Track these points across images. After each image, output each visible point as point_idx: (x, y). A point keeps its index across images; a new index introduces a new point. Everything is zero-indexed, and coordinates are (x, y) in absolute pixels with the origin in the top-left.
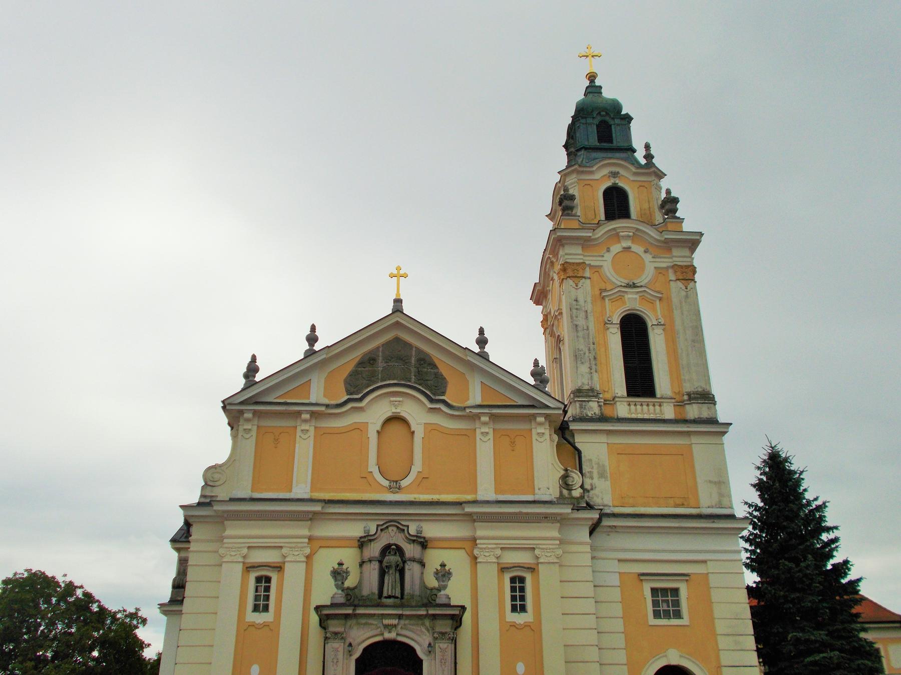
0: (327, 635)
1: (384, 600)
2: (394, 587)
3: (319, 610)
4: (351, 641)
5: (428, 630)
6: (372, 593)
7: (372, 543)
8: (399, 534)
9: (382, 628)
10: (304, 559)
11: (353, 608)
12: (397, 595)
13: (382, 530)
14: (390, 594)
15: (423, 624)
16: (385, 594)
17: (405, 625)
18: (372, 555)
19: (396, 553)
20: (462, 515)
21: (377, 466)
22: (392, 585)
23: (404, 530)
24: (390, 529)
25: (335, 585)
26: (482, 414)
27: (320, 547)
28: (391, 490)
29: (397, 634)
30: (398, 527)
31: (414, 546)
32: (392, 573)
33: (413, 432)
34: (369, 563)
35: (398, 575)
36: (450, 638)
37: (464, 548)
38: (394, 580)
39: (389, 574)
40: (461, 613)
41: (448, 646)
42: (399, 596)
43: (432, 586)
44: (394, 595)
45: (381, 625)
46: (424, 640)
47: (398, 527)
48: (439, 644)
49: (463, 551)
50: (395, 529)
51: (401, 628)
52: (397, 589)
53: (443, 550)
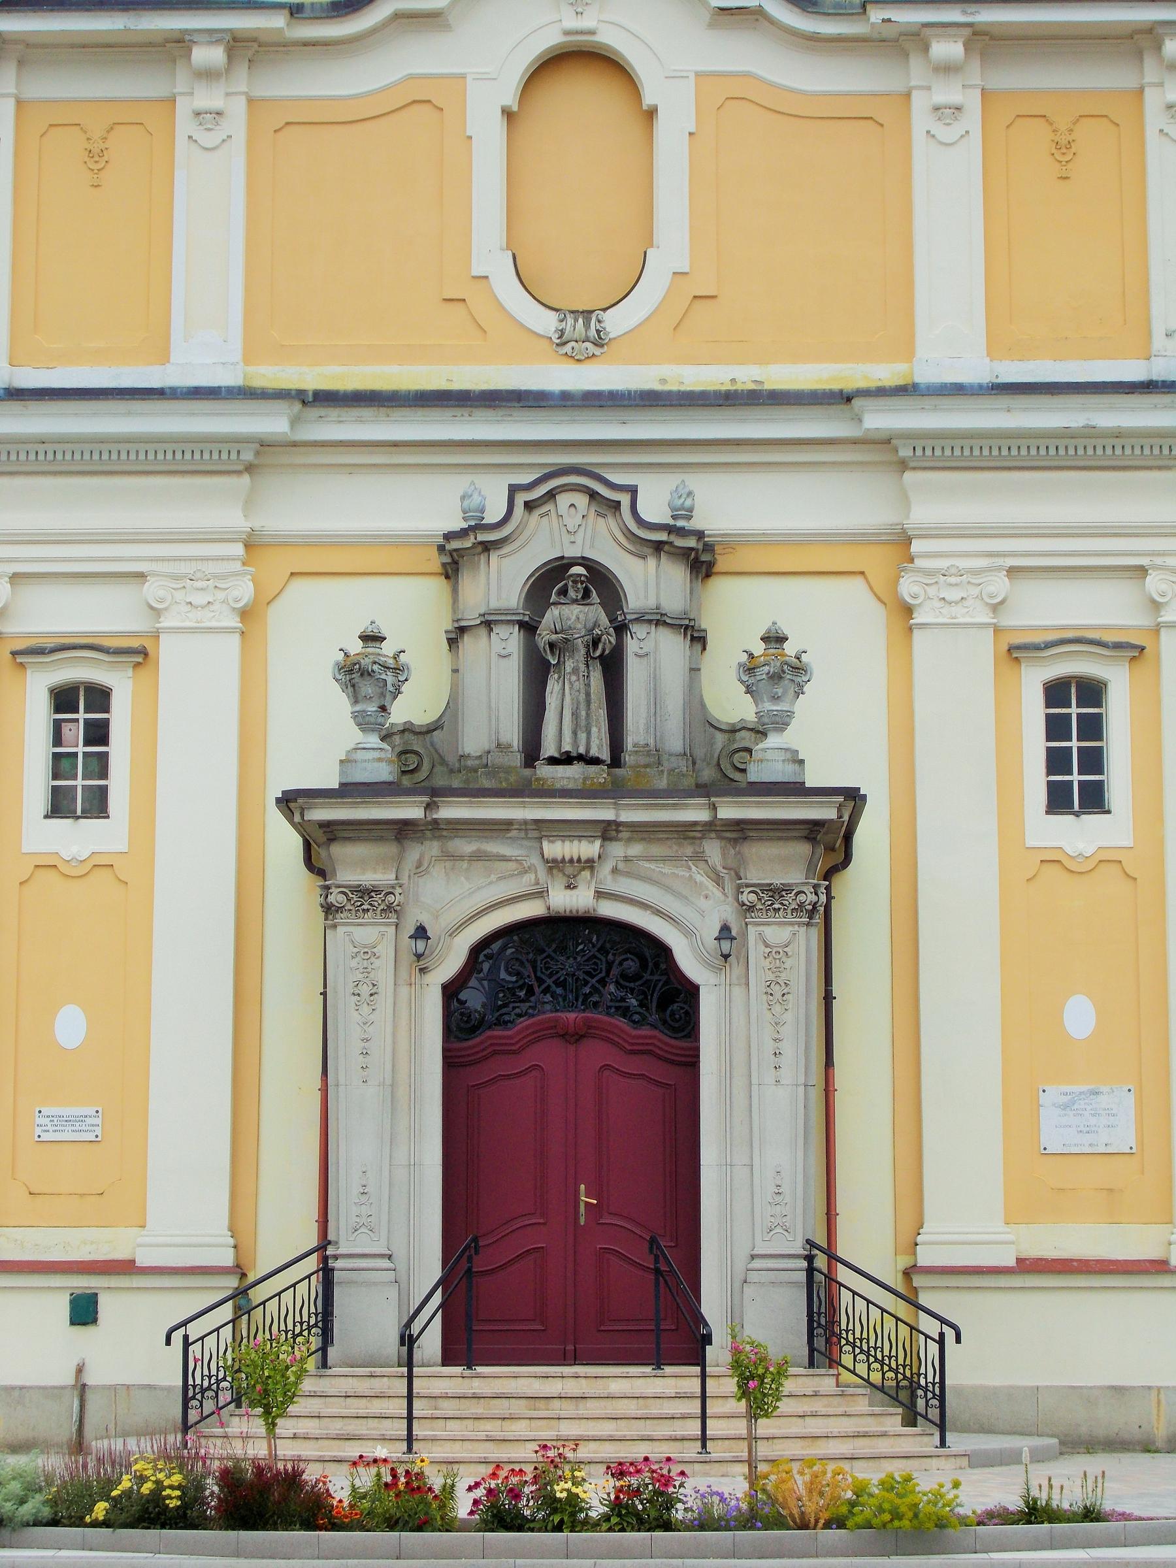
0: (331, 899)
1: (545, 771)
2: (583, 723)
4: (425, 919)
5: (718, 880)
6: (499, 745)
7: (494, 557)
8: (601, 520)
10: (234, 622)
11: (426, 799)
12: (594, 752)
13: (529, 506)
14: (567, 747)
15: (699, 857)
16: (549, 748)
17: (627, 859)
18: (494, 604)
19: (587, 594)
20: (855, 442)
21: (510, 253)
22: (575, 715)
23: (619, 502)
24: (564, 500)
26: (940, 31)
28: (567, 348)
29: (599, 895)
30: (593, 495)
31: (658, 566)
32: (575, 671)
33: (651, 114)
34: (483, 631)
37: (862, 573)
38: (582, 697)
39: (562, 678)
44: (582, 750)
45: (535, 860)
46: (702, 913)
47: (593, 495)
50: (582, 500)
51: (615, 871)
52: (594, 730)
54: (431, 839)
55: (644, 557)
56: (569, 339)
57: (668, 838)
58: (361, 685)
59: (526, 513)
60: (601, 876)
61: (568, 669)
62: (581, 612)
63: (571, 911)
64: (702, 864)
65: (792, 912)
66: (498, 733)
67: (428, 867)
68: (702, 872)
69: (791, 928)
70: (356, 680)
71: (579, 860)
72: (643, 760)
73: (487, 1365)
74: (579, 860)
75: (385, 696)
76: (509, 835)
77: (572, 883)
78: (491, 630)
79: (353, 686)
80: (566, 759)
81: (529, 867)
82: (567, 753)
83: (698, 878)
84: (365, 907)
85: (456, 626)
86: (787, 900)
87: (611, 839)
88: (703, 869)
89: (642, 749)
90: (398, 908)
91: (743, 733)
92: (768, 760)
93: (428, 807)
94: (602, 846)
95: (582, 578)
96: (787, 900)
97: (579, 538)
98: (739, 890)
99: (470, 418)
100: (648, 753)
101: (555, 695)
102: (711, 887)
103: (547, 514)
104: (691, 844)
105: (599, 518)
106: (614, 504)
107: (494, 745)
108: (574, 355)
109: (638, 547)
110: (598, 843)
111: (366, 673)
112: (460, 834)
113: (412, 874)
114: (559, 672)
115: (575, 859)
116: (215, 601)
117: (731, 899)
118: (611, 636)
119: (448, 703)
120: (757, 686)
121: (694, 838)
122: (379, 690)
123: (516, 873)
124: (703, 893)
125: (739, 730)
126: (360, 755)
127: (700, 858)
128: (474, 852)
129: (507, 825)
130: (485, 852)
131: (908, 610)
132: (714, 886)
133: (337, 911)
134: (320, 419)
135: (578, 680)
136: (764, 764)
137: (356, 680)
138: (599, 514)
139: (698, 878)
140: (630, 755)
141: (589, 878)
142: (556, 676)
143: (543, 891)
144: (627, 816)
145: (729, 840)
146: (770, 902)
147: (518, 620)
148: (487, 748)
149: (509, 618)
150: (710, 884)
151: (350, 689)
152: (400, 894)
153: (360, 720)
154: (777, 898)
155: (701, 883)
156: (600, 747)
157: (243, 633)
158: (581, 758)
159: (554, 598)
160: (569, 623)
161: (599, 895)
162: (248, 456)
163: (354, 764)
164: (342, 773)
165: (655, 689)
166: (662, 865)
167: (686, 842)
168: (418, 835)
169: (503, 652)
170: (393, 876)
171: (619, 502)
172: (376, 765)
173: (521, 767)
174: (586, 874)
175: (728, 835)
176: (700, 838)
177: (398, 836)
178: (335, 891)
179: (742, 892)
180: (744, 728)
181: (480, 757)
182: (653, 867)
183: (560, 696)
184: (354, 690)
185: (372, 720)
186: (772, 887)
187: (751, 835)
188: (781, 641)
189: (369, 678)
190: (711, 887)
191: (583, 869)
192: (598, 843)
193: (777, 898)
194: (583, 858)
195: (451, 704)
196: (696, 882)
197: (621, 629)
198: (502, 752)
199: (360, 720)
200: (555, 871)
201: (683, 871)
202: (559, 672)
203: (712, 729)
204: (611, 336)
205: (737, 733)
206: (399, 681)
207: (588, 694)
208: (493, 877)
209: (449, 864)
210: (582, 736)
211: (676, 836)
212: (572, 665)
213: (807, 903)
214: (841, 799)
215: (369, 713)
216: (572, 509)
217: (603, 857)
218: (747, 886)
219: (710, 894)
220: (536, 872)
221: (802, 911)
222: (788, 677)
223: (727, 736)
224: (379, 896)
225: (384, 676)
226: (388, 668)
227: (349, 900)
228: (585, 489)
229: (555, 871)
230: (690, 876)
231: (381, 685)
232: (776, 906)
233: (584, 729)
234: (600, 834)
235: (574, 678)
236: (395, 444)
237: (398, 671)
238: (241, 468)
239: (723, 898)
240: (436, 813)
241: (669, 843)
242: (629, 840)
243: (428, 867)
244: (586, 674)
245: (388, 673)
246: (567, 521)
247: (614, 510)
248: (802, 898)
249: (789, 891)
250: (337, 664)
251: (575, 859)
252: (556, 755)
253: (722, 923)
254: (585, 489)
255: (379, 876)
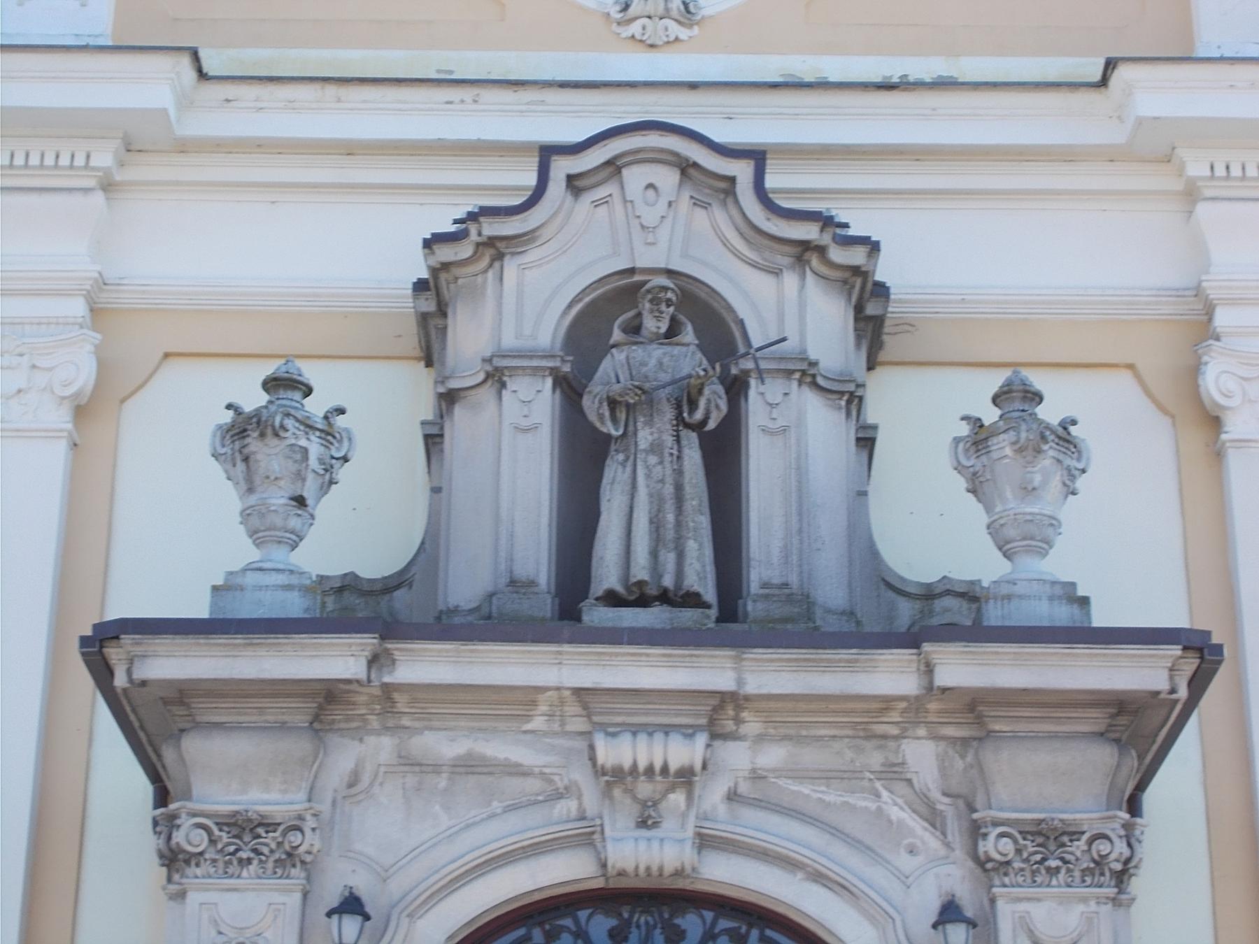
0: (179, 837)
1: (597, 615)
2: (670, 534)
3: (114, 654)
4: (362, 884)
5: (934, 819)
6: (513, 582)
7: (511, 267)
8: (700, 213)
9: (591, 800)
10: (61, 418)
11: (369, 641)
12: (692, 581)
13: (575, 184)
14: (640, 571)
15: (894, 773)
16: (607, 575)
17: (756, 776)
18: (509, 340)
19: (673, 332)
20: (1110, 155)
22: (656, 524)
23: (732, 180)
24: (635, 177)
25: (246, 515)
27: (167, 355)
28: (635, 28)
29: (705, 842)
30: (686, 168)
31: (802, 287)
32: (656, 448)
34: (487, 393)
35: (693, 457)
36: (1100, 862)
37: (1130, 367)
38: (669, 489)
39: (631, 460)
40: (1183, 693)
41: (1089, 920)
42: (710, 595)
43: (929, 576)
44: (668, 581)
45: (580, 775)
46: (904, 879)
47: (686, 168)
48: (1022, 907)
49: (1124, 380)
50: (667, 178)
51: (733, 796)
52: (691, 545)
53: (1051, 79)
54: (378, 733)
55: (777, 273)
56: (638, 14)
57: (834, 737)
58: (259, 457)
59: (569, 198)
60: (706, 805)
61: (643, 445)
62: (665, 354)
63: (648, 869)
64: (901, 787)
65: (1083, 877)
66: (512, 560)
67: (371, 784)
68: (900, 801)
69: (1081, 908)
70: (252, 448)
71: (665, 770)
72: (778, 610)
73: (552, 898)
74: (665, 770)
75: (304, 480)
76: (529, 727)
77: (650, 817)
78: (503, 385)
79: (246, 459)
80: (639, 597)
81: (566, 788)
82: (641, 584)
83: (895, 813)
84: (243, 855)
85: (442, 390)
86: (1072, 853)
87: (725, 737)
88: (902, 797)
89: (777, 592)
90: (308, 858)
91: (948, 602)
92: (1020, 597)
93: (373, 661)
94: (708, 746)
95: (670, 295)
96: (1072, 853)
97: (663, 234)
98: (976, 831)
99: (475, 107)
100: (790, 599)
101: (618, 488)
102: (919, 831)
103: (604, 202)
104: (880, 747)
105: (698, 210)
106: (723, 185)
107: (504, 581)
108: (644, 39)
109: (767, 254)
110: (701, 739)
111: (269, 431)
112: (436, 724)
113: (339, 798)
114: (626, 450)
115: (658, 766)
116: (30, 388)
117: (959, 853)
118: (720, 397)
119: (423, 543)
120: (992, 471)
121: (885, 737)
122: (293, 467)
123: (540, 798)
124: (906, 842)
125: (941, 595)
126: (251, 579)
127: (896, 776)
128: (459, 758)
129: (526, 697)
130: (483, 758)
131: (1214, 422)
132: (926, 829)
133: (187, 862)
134: (226, 105)
135: (661, 463)
136: (1015, 602)
137: (252, 448)
138: (697, 203)
139: (895, 813)
140: (754, 601)
141: (683, 805)
142: (621, 457)
143: (593, 833)
144: (755, 684)
145: (952, 741)
146: (1038, 857)
147: (552, 369)
148: (490, 589)
149: (535, 363)
150: (917, 825)
151: (241, 466)
152: (313, 829)
153: (255, 522)
154: (1052, 848)
155: (901, 823)
156: (701, 578)
157: (75, 445)
158: (665, 598)
159: (617, 335)
160: (644, 369)
161: (705, 842)
162: (104, 158)
163: (238, 593)
164: (214, 605)
165: (800, 490)
166: (823, 788)
167: (869, 745)
168: (354, 725)
169: (525, 423)
170: (302, 796)
171: (732, 180)
172: (281, 595)
173: (552, 619)
174: (677, 798)
175: (950, 731)
176: (896, 738)
177: (316, 725)
178: (186, 822)
179: (985, 835)
180: (948, 592)
181: (477, 609)
182: (806, 792)
183: (628, 488)
184: (248, 467)
185: (278, 521)
186: (1043, 826)
187: (997, 728)
188: (1032, 400)
189: (275, 441)
190: (919, 831)
191: (672, 789)
192: (701, 739)
193: (1052, 848)
194: (673, 767)
195: (427, 546)
196: (890, 821)
197: (736, 388)
198: (517, 593)
199: (255, 522)
200: (617, 792)
201: (865, 799)
202: (626, 450)
203: (891, 594)
204: (705, 12)
205: (936, 601)
206: (333, 458)
207: (679, 488)
208: (496, 806)
209: (411, 780)
210: (669, 559)
211: (850, 733)
212: (650, 438)
213: (1113, 856)
214: (1176, 650)
215: (272, 508)
216: (651, 192)
217: (710, 767)
218: (996, 824)
219: (919, 843)
220: (580, 797)
221: (1102, 874)
222: (1051, 453)
223: (918, 605)
224: (271, 834)
225: (303, 442)
226: (311, 427)
227: (212, 842)
228: (670, 158)
229: (617, 792)
230: (879, 809)
231: (298, 457)
232: (1053, 863)
233: (671, 545)
234: (703, 721)
235: (653, 460)
236: (350, 149)
237: (329, 438)
238: (91, 183)
239: (943, 852)
240: (391, 673)
241: (837, 745)
242: (760, 739)
243: (371, 784)
244: (675, 452)
245: (312, 438)
246: (641, 209)
247: (722, 196)
248: (1103, 847)
249: (1076, 835)
250: (220, 427)
251: (658, 766)
252: (619, 588)
253: (945, 899)
254: (670, 158)
255: (274, 796)
